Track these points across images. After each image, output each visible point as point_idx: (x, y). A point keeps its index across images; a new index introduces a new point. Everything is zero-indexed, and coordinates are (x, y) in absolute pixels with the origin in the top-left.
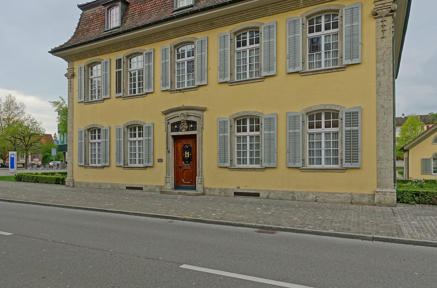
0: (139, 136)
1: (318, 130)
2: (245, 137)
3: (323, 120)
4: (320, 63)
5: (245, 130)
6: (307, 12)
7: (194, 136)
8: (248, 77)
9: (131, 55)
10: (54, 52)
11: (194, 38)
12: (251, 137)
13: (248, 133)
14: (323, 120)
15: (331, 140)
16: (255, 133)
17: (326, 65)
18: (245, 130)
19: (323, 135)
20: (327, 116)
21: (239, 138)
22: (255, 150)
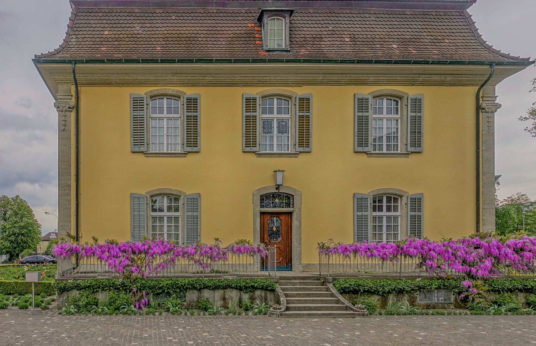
0: (389, 209)
1: (380, 214)
2: (381, 218)
3: (385, 204)
4: (272, 146)
5: (380, 209)
6: (151, 91)
7: (291, 213)
8: (385, 151)
9: (157, 96)
10: (38, 61)
11: (182, 92)
12: (388, 218)
13: (384, 213)
14: (385, 204)
15: (392, 224)
16: (173, 214)
17: (387, 150)
18: (380, 209)
19: (385, 218)
20: (389, 200)
21: (375, 218)
22: (392, 232)
